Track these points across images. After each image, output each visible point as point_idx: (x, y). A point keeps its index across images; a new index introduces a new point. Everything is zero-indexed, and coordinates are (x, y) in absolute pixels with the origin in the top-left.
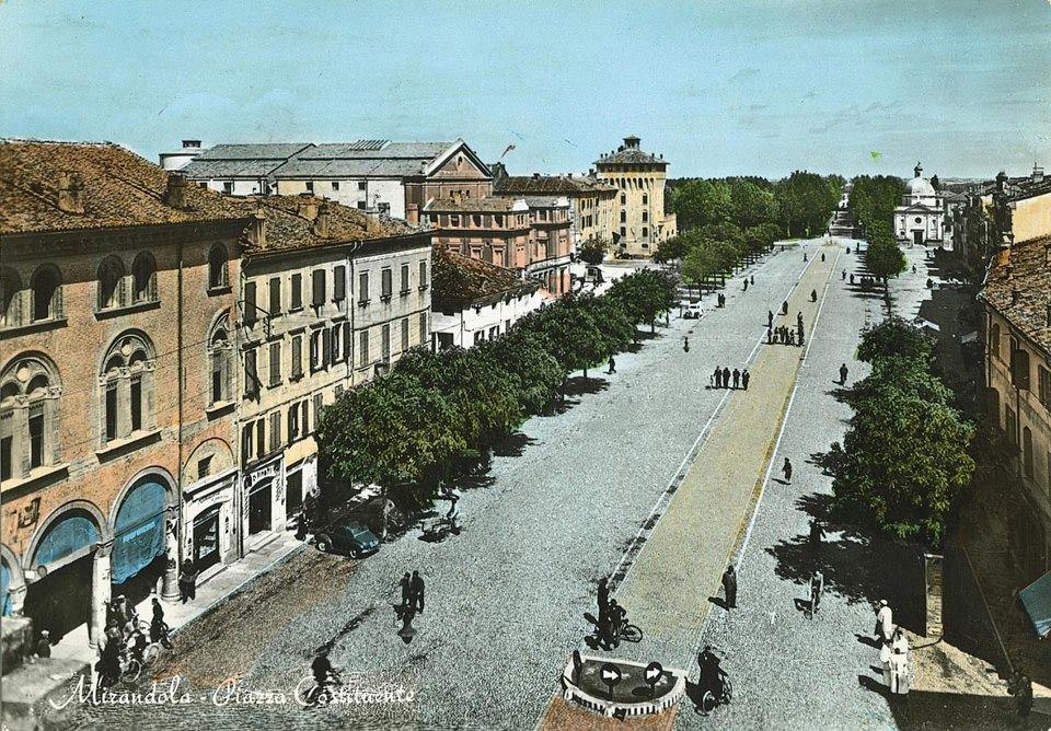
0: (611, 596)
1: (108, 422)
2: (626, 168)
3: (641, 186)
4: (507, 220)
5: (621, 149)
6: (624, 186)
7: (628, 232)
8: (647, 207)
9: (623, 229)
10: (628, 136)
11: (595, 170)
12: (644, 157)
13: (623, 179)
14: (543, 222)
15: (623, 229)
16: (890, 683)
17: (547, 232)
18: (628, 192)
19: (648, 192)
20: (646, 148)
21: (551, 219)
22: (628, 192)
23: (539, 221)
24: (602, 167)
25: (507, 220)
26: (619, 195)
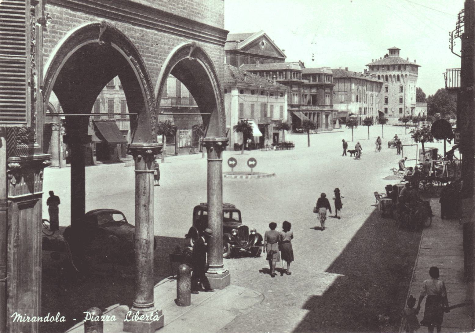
0: (130, 160)
1: (139, 184)
2: (388, 67)
3: (399, 79)
4: (286, 75)
5: (386, 56)
6: (387, 80)
7: (389, 111)
8: (403, 94)
9: (386, 109)
10: (392, 47)
11: (368, 70)
12: (403, 61)
13: (386, 76)
14: (315, 83)
15: (386, 109)
16: (319, 106)
17: (318, 89)
18: (390, 84)
19: (404, 85)
20: (403, 56)
21: (319, 81)
22: (390, 84)
23: (312, 82)
24: (372, 67)
25: (286, 75)
26: (384, 86)
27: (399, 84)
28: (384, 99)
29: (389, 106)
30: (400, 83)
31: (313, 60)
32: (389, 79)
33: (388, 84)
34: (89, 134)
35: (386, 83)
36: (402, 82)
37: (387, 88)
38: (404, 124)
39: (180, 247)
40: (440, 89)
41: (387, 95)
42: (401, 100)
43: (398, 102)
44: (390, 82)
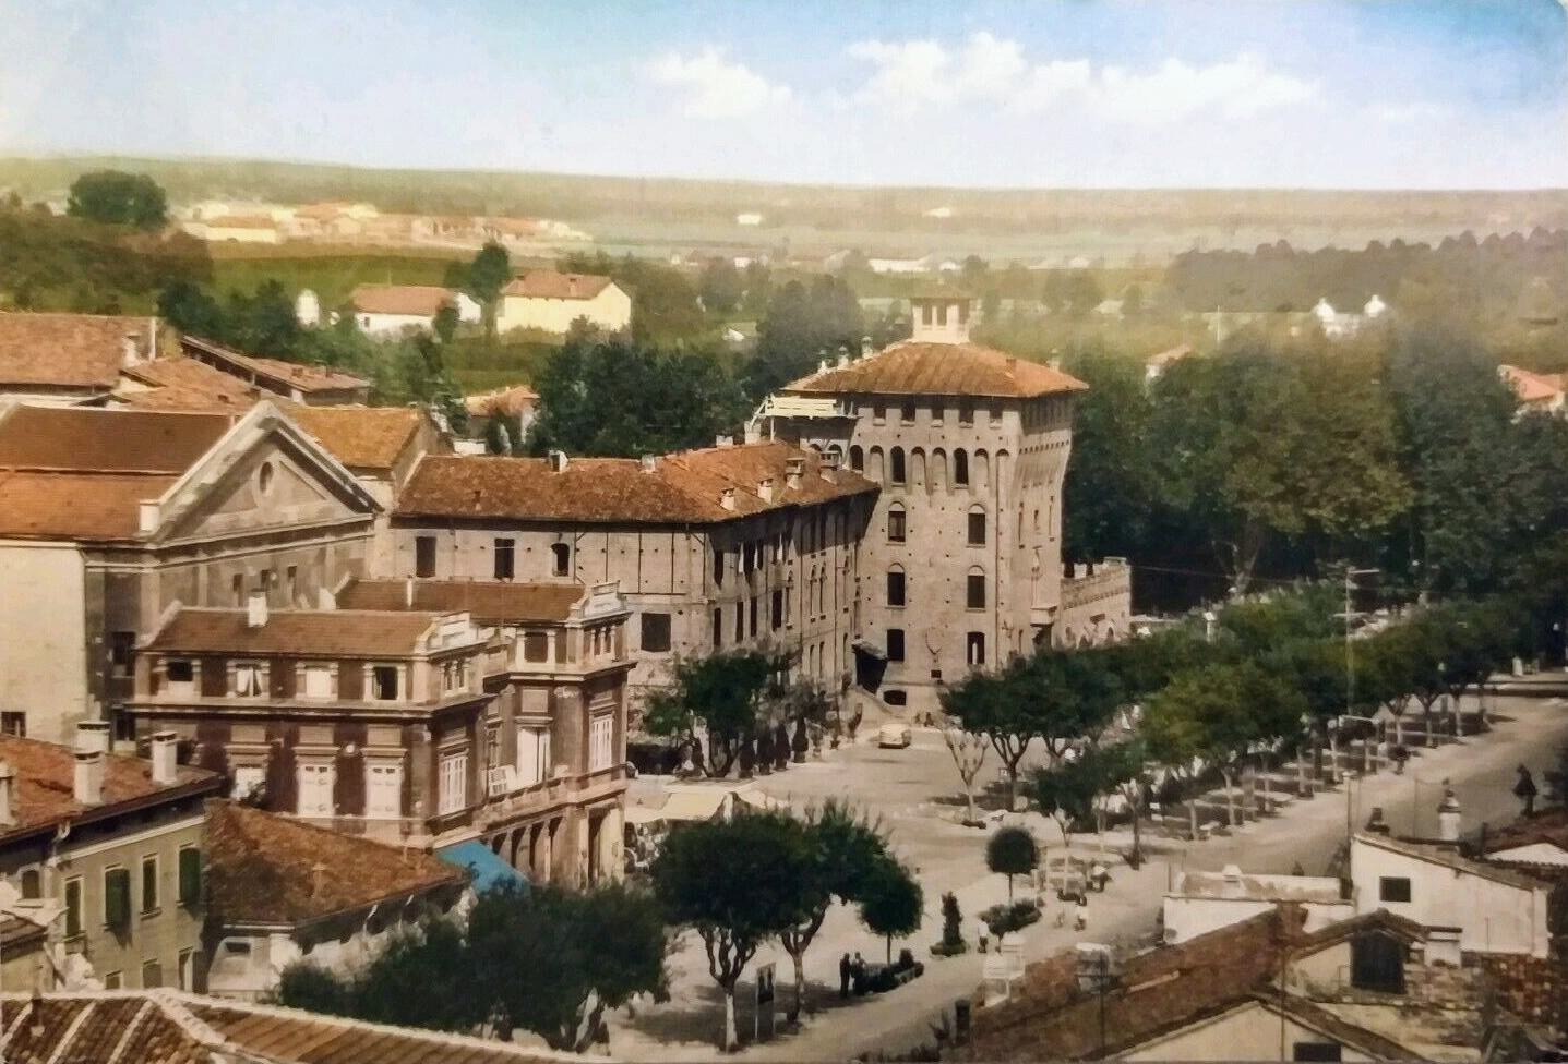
3: (962, 476)
6: (899, 474)
9: (896, 639)
15: (896, 639)
18: (915, 501)
22: (915, 501)
27: (963, 497)
28: (883, 580)
29: (912, 620)
30: (973, 493)
31: (1022, 547)
32: (913, 465)
33: (908, 499)
34: (888, 410)
35: (899, 492)
36: (983, 492)
37: (898, 517)
38: (1279, 1010)
39: (765, 360)
40: (525, 326)
41: (898, 552)
42: (976, 592)
43: (962, 599)
44: (920, 491)
